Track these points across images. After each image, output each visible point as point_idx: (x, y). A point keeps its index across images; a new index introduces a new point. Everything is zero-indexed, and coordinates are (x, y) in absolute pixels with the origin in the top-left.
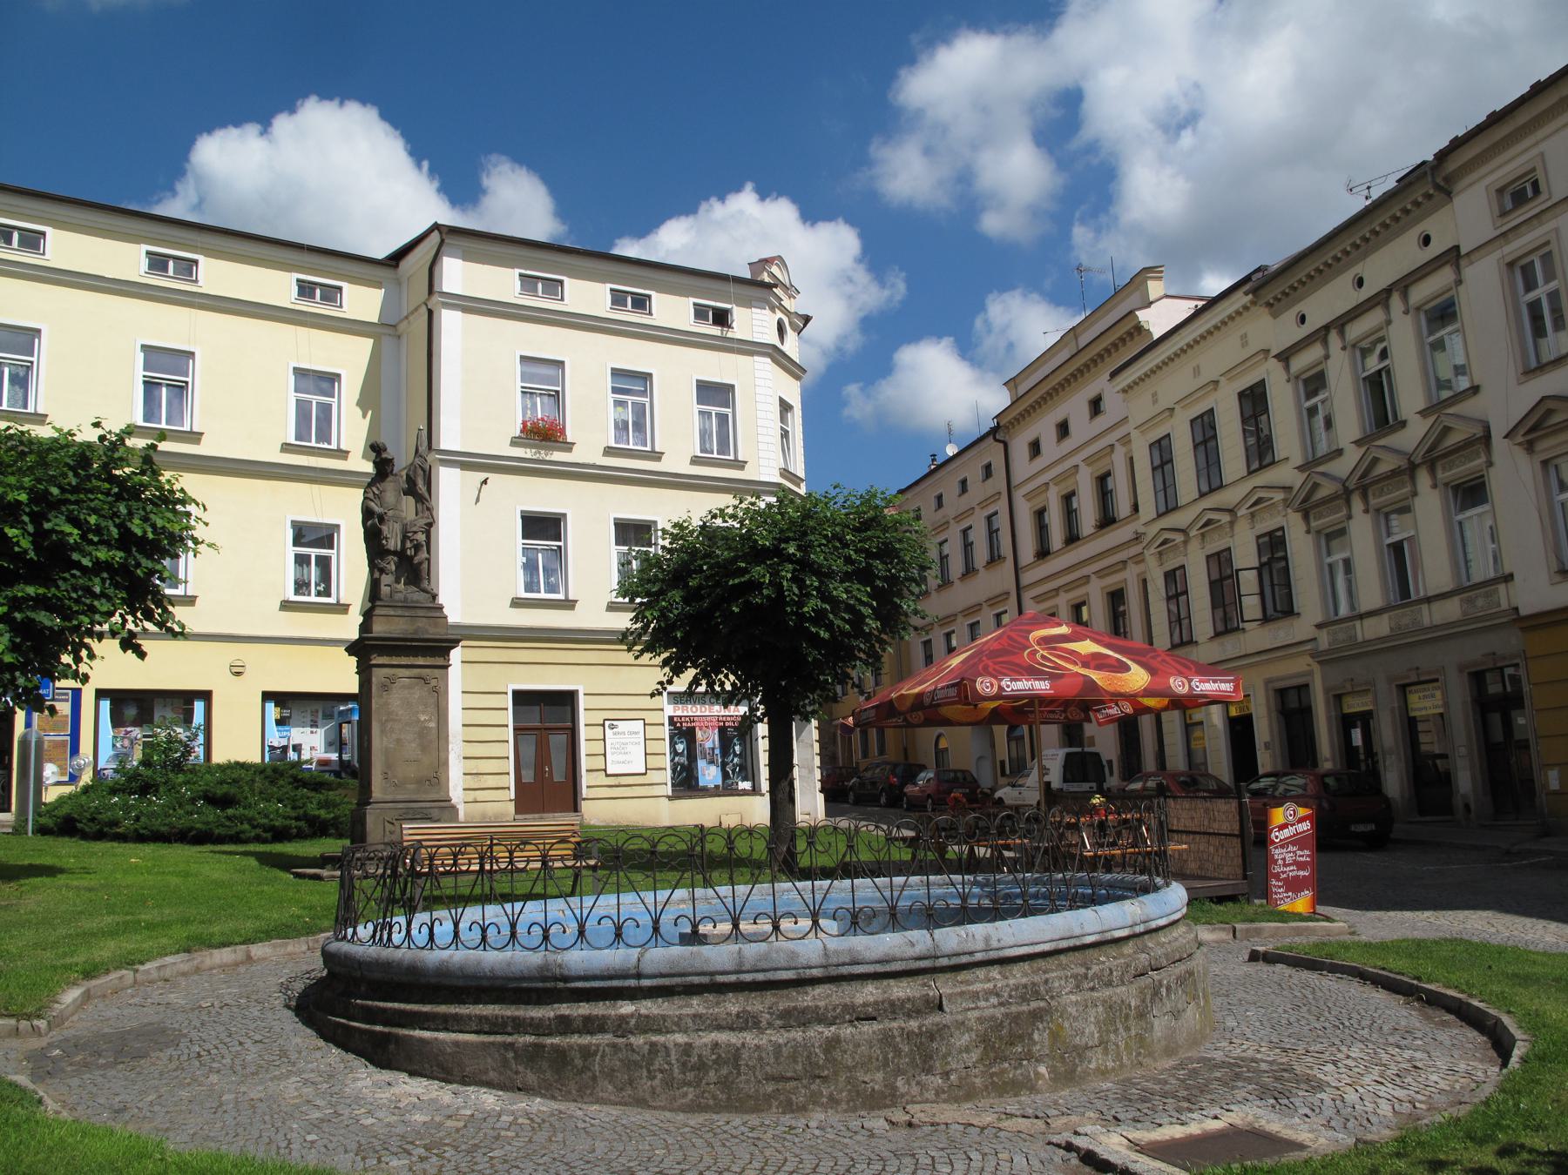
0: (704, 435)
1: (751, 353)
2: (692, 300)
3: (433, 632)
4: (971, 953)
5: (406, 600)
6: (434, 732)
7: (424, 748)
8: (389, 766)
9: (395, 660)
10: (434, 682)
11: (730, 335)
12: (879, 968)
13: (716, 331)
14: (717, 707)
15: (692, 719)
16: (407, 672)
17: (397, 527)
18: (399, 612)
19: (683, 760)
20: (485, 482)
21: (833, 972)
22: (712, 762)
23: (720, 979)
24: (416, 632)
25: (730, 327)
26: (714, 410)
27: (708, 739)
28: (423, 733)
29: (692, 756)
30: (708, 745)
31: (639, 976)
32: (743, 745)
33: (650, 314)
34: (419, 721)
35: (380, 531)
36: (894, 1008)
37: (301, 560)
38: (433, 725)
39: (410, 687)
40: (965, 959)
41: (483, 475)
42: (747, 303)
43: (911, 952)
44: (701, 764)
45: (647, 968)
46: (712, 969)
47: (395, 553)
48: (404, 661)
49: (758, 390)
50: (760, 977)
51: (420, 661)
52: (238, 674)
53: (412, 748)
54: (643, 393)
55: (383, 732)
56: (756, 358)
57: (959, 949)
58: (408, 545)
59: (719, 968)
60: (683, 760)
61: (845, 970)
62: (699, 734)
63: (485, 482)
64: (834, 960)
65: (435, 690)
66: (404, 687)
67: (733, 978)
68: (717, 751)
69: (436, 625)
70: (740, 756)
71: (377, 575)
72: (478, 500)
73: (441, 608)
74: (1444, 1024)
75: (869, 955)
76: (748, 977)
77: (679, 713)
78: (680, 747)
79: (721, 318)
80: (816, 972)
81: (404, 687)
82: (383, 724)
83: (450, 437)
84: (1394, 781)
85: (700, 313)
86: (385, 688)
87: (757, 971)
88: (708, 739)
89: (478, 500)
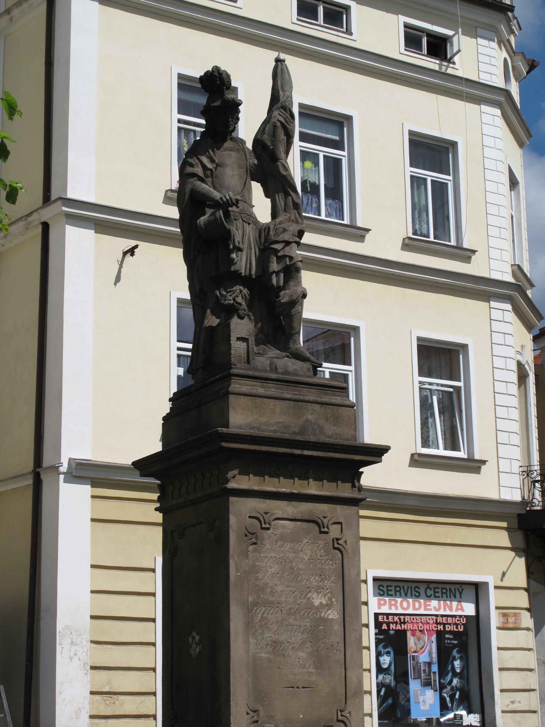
0: (418, 210)
1: (478, 100)
2: (404, 19)
3: (330, 432)
5: (275, 369)
6: (338, 628)
7: (320, 661)
8: (260, 695)
9: (271, 485)
10: (334, 531)
11: (450, 71)
13: (432, 64)
14: (434, 603)
15: (402, 618)
17: (250, 231)
18: (273, 390)
19: (389, 679)
20: (131, 251)
22: (427, 684)
24: (303, 430)
25: (450, 61)
26: (430, 176)
27: (423, 649)
28: (317, 630)
29: (402, 676)
30: (423, 658)
32: (465, 659)
33: (349, 32)
34: (310, 606)
35: (227, 235)
37: (417, 183)
38: (334, 615)
39: (294, 538)
41: (129, 243)
42: (473, 31)
44: (414, 685)
47: (246, 281)
48: (284, 485)
49: (488, 152)
51: (313, 488)
53: (298, 662)
54: (338, 145)
55: (249, 625)
56: (485, 108)
58: (274, 266)
60: (389, 679)
62: (411, 642)
63: (131, 251)
65: (337, 546)
66: (283, 538)
68: (435, 668)
69: (336, 420)
70: (460, 675)
71: (212, 321)
72: (118, 279)
77: (385, 609)
78: (386, 660)
79: (438, 47)
81: (283, 538)
82: (249, 610)
83: (82, 182)
85: (412, 39)
86: (252, 537)
88: (423, 649)
89: (118, 279)
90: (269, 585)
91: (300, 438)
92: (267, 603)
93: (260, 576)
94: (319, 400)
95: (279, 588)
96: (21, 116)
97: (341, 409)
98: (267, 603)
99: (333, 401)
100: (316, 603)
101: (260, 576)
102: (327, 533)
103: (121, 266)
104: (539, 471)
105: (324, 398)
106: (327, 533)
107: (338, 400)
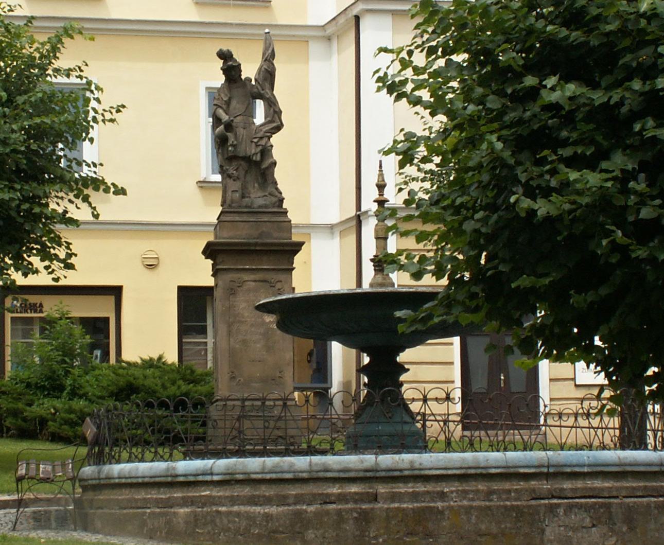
3: (276, 237)
4: (401, 470)
12: (342, 475)
16: (252, 277)
21: (315, 475)
23: (254, 476)
31: (212, 474)
36: (342, 498)
40: (397, 474)
43: (361, 466)
45: (216, 470)
46: (248, 471)
50: (274, 476)
52: (150, 267)
57: (393, 467)
59: (252, 470)
61: (321, 475)
64: (315, 468)
67: (260, 476)
73: (285, 213)
74: (54, 400)
75: (335, 467)
76: (268, 476)
80: (305, 475)
81: (249, 290)
84: (29, 24)
87: (272, 473)
90: (342, 444)
91: (259, 241)
92: (240, 322)
93: (236, 309)
94: (270, 220)
95: (246, 315)
96: (102, 92)
97: (282, 224)
98: (240, 322)
99: (278, 220)
100: (268, 320)
101: (236, 309)
102: (274, 286)
103: (259, 281)
104: (617, 432)
105: (493, 447)
106: (274, 286)
107: (282, 219)
